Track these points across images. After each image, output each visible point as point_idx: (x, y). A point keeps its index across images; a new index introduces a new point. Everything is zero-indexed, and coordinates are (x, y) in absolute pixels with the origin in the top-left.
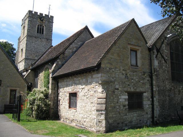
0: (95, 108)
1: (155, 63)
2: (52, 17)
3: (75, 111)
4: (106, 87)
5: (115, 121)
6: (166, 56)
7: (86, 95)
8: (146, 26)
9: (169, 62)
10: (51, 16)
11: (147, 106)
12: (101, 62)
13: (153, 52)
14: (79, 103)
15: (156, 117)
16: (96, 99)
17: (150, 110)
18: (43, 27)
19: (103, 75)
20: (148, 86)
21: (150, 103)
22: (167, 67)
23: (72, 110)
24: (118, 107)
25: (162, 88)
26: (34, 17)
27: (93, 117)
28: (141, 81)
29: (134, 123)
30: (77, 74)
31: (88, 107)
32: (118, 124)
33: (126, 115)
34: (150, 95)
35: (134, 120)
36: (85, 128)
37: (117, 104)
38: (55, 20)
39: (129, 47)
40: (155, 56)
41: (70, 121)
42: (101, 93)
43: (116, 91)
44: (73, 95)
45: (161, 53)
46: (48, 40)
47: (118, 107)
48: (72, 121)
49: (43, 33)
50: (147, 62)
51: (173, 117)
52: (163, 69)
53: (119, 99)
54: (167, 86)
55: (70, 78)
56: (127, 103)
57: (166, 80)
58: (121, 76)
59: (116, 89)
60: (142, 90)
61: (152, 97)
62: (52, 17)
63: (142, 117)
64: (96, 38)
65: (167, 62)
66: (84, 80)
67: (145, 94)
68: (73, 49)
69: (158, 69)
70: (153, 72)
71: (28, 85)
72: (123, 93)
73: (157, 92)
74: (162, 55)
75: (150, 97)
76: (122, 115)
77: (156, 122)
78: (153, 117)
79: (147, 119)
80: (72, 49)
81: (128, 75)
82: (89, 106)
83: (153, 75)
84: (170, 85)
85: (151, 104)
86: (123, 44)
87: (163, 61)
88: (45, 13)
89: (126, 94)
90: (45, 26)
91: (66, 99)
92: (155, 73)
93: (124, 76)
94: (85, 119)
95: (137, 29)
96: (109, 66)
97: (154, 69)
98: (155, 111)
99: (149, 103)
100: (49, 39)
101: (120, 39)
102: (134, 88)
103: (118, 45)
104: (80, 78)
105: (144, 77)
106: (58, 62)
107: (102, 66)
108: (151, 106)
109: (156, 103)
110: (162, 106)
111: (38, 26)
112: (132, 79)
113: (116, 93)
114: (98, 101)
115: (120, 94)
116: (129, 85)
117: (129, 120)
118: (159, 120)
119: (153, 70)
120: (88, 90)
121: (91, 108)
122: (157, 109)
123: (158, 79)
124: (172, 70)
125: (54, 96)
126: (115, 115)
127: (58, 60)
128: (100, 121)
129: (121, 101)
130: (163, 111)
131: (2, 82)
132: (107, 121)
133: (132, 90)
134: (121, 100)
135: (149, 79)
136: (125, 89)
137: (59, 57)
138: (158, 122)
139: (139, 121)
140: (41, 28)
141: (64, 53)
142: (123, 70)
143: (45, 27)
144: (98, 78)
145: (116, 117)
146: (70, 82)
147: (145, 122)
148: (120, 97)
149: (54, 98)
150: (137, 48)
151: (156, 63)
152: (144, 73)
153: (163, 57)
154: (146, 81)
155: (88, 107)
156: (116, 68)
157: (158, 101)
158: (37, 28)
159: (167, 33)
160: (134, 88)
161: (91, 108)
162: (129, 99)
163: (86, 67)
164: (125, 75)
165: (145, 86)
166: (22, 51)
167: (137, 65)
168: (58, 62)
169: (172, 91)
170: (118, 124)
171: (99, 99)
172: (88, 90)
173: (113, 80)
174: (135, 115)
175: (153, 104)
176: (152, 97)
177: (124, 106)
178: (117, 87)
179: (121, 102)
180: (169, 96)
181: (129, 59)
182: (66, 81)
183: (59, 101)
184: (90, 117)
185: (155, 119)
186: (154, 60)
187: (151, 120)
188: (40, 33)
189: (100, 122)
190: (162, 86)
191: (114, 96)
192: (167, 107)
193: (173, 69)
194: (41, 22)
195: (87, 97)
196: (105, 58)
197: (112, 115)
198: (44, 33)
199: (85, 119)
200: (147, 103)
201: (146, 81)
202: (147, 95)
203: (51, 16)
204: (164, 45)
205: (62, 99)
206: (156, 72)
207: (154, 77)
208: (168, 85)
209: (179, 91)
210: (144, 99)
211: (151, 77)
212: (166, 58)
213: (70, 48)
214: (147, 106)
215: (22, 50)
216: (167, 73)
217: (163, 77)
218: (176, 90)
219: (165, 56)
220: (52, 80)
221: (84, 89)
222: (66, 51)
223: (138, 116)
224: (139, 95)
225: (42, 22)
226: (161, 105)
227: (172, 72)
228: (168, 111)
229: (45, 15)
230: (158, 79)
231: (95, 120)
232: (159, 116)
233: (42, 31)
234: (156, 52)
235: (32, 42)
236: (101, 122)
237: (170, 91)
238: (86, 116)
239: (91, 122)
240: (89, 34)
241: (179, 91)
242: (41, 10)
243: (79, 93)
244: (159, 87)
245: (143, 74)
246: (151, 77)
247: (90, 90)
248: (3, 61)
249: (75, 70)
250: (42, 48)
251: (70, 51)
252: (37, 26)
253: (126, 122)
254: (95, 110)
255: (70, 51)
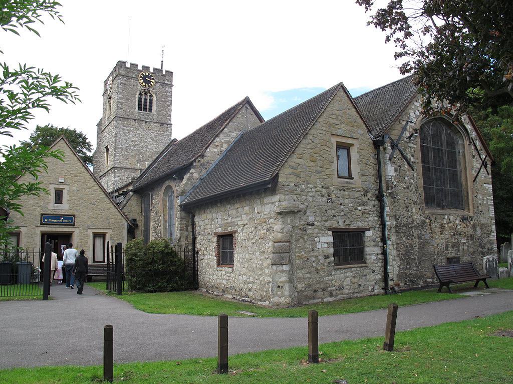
0: (269, 262)
1: (204, 216)
2: (170, 73)
3: (231, 269)
4: (289, 221)
5: (309, 286)
6: (413, 156)
7: (252, 237)
8: (372, 92)
9: (419, 167)
10: (166, 71)
11: (374, 257)
12: (278, 173)
13: (385, 149)
14: (238, 256)
15: (393, 280)
16: (270, 243)
17: (380, 264)
18: (151, 96)
19: (283, 197)
20: (373, 219)
21: (380, 252)
22: (415, 177)
23: (224, 269)
24: (313, 259)
25: (404, 221)
26: (130, 75)
27: (266, 280)
28: (360, 208)
29: (347, 291)
30: (233, 198)
31: (256, 262)
32: (315, 291)
33: (331, 274)
34: (380, 234)
35: (348, 285)
36: (250, 302)
37: (312, 254)
38: (176, 80)
39: (334, 140)
40: (387, 156)
41: (221, 291)
42: (279, 232)
43: (310, 227)
44: (226, 241)
45: (400, 151)
46: (162, 124)
47: (313, 259)
48: (224, 291)
49: (151, 110)
50: (371, 170)
51: (429, 280)
52: (405, 183)
53: (316, 243)
54: (415, 217)
55: (219, 205)
56: (332, 250)
57: (413, 205)
58: (319, 199)
59: (309, 224)
60: (360, 224)
61: (383, 240)
62: (170, 73)
63: (364, 278)
64: (267, 122)
65: (415, 168)
66: (246, 208)
67: (368, 234)
68: (222, 147)
69: (395, 183)
70: (384, 188)
71: (128, 224)
72: (323, 232)
73: (393, 230)
74: (402, 154)
75: (378, 239)
76: (322, 273)
77: (392, 289)
78: (385, 278)
79: (373, 283)
80: (219, 148)
81: (333, 197)
82: (257, 258)
83: (385, 194)
84: (420, 215)
85: (382, 254)
86: (321, 135)
87: (406, 166)
88: (153, 64)
89: (330, 233)
90: (156, 94)
91: (211, 248)
92: (389, 191)
93: (325, 199)
94: (250, 285)
95: (349, 102)
96: (293, 179)
97: (387, 182)
98: (389, 267)
99: (378, 250)
100: (165, 124)
101: (315, 126)
102: (345, 221)
103: (311, 137)
104: (238, 205)
105: (365, 199)
106: (192, 174)
107: (280, 180)
108: (380, 257)
109: (392, 252)
110: (406, 257)
111: (140, 94)
112: (341, 204)
113: (309, 232)
114: (274, 247)
115: (317, 233)
116: (334, 216)
117: (337, 285)
118: (398, 285)
119: (384, 185)
120: (256, 228)
121: (261, 262)
122: (394, 263)
123: (394, 202)
124: (425, 183)
125: (186, 244)
126: (309, 275)
127: (192, 171)
128: (280, 285)
129: (320, 247)
130: (408, 267)
131: (77, 219)
132: (294, 286)
133: (342, 225)
134: (319, 246)
135: (376, 202)
136: (327, 224)
137: (194, 164)
138: (396, 288)
139: (356, 286)
140: (145, 99)
141: (203, 156)
142: (323, 187)
143: (154, 95)
144: (273, 203)
145: (309, 278)
146: (219, 214)
147: (370, 288)
148: (317, 240)
149: (187, 247)
150: (350, 141)
151: (390, 171)
152: (366, 193)
153: (404, 157)
154: (369, 207)
155: (256, 262)
156: (308, 183)
157: (395, 246)
158: (137, 99)
159: (413, 107)
160: (345, 221)
161: (261, 262)
162: (335, 244)
163: (251, 182)
164: (326, 195)
165: (367, 218)
166: (107, 151)
167: (350, 177)
168: (192, 174)
169: (426, 226)
170: (315, 291)
171: (276, 244)
172: (256, 228)
173: (302, 206)
174: (349, 274)
175: (385, 253)
176: (383, 240)
177: (326, 257)
178: (311, 219)
179: (320, 250)
180: (419, 238)
181: (334, 165)
182: (211, 212)
183: (197, 253)
184: (261, 279)
185: (391, 283)
186: (385, 163)
187: (382, 284)
188: (145, 109)
189: (279, 287)
190: (404, 217)
191: (306, 237)
192: (415, 258)
193: (427, 180)
194: (147, 85)
195: (253, 241)
196: (286, 164)
197: (303, 274)
198: (154, 108)
199: (250, 285)
200: (372, 252)
201: (369, 207)
202: (371, 235)
203: (166, 71)
204: (406, 132)
205: (203, 249)
206: (390, 188)
207: (386, 200)
208: (416, 214)
209: (442, 227)
210: (367, 244)
211: (380, 198)
212: (412, 159)
213: (216, 144)
214: (374, 257)
215: (107, 148)
216: (414, 190)
217: (407, 199)
218: (433, 225)
219: (409, 156)
220: (181, 211)
221: (246, 226)
222: (208, 150)
223: (354, 277)
224: (358, 234)
225: (149, 86)
226: (402, 254)
227: (425, 188)
228: (418, 267)
229: (155, 69)
230: (394, 202)
231: (270, 285)
232: (399, 276)
233: (142, 105)
234: (390, 148)
235: (129, 131)
236: (282, 287)
237: (422, 226)
238: (251, 279)
239: (262, 291)
240: (253, 113)
241: (442, 227)
242: (147, 59)
243: (237, 235)
244: (396, 219)
245: (362, 193)
246: (380, 198)
247: (259, 228)
248: (77, 176)
249: (228, 189)
250: (151, 142)
251: (216, 150)
252: (137, 96)
253: (331, 288)
254: (269, 265)
255: (216, 150)
